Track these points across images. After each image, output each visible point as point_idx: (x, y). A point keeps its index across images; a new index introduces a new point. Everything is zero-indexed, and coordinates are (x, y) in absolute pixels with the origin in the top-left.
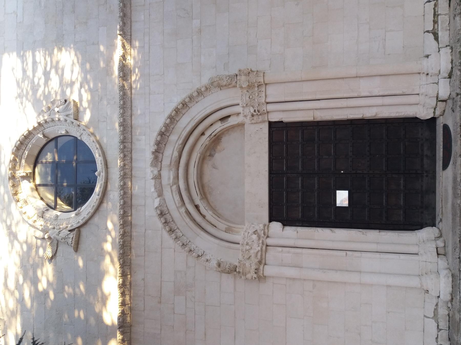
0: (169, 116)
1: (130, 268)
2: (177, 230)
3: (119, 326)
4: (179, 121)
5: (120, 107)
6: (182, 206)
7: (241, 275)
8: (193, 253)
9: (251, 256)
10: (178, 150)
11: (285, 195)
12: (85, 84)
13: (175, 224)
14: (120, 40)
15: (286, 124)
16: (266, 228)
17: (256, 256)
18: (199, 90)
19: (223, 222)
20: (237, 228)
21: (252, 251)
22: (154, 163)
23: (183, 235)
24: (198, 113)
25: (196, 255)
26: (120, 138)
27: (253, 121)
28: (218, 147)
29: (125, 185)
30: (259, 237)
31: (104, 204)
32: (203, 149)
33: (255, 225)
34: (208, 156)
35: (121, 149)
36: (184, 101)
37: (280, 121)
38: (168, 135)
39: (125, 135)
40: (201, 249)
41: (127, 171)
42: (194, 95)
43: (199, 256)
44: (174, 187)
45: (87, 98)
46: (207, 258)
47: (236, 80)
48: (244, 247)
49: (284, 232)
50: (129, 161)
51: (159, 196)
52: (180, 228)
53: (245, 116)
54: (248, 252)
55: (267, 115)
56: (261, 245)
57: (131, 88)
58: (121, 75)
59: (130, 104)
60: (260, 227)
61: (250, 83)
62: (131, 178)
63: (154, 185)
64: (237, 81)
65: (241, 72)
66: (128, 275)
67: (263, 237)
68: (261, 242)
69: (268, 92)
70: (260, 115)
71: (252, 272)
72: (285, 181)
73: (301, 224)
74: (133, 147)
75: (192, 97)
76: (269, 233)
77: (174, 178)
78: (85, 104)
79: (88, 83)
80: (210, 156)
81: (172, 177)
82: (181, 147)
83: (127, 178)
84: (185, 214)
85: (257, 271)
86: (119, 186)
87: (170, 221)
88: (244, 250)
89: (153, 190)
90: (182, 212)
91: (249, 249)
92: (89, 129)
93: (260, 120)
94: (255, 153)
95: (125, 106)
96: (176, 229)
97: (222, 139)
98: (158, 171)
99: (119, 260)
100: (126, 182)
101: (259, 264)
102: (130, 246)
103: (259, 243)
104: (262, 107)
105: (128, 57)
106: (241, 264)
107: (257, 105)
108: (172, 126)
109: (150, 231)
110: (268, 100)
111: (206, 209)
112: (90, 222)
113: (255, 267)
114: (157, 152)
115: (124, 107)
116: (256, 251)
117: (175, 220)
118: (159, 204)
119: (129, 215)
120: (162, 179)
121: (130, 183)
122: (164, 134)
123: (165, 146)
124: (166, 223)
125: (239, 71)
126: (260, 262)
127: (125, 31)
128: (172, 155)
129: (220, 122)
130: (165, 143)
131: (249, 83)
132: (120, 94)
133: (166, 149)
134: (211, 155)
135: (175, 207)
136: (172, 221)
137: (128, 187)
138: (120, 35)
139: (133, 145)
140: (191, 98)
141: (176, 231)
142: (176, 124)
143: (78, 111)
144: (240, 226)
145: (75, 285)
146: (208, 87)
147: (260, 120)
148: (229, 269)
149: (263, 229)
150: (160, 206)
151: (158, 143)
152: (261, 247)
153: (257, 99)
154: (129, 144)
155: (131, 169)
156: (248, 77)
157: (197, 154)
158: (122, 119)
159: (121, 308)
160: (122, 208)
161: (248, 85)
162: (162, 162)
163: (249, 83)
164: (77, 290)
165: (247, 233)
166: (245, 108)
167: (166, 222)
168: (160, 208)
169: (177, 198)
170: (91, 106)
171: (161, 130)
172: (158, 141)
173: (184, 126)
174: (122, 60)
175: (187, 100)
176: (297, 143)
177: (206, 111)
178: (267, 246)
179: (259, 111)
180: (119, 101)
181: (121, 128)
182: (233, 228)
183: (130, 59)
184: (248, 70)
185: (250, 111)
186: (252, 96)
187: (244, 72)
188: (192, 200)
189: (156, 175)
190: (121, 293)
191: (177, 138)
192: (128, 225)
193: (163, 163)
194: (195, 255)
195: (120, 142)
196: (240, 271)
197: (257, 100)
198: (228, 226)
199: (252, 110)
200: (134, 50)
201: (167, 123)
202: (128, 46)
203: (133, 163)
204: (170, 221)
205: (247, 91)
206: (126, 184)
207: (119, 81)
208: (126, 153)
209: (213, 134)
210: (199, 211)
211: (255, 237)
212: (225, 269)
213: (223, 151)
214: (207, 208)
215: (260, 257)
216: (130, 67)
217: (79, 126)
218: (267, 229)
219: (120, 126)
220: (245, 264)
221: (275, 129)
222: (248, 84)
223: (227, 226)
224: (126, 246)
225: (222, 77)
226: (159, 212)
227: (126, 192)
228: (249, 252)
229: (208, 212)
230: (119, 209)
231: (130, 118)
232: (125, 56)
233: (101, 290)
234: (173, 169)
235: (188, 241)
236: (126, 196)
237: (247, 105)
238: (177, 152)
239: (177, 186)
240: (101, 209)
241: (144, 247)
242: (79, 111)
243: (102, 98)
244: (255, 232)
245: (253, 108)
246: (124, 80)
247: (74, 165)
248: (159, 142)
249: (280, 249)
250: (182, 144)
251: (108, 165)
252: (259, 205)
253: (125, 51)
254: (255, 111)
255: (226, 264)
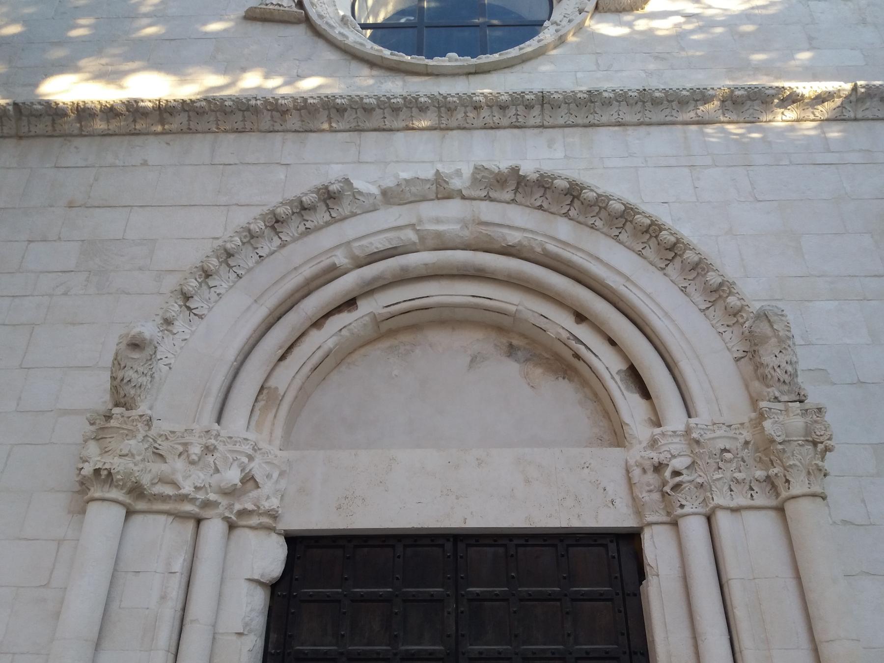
0: (632, 209)
1: (182, 132)
2: (277, 242)
3: (21, 104)
4: (617, 244)
5: (644, 90)
6: (354, 258)
7: (98, 422)
8: (198, 280)
9: (166, 463)
10: (525, 243)
11: (381, 590)
12: (697, 24)
13: (296, 235)
14: (839, 88)
15: (635, 595)
16: (266, 520)
17: (163, 480)
18: (729, 288)
19: (298, 382)
20: (273, 424)
21: (180, 464)
22: (483, 177)
23: (260, 257)
24: (649, 296)
25: (191, 289)
26: (555, 92)
27: (636, 472)
28: (539, 371)
29: (418, 110)
30: (230, 493)
31: (370, 70)
32: (533, 321)
33: (277, 482)
34: (510, 340)
35: (523, 97)
36: (687, 247)
37: (647, 569)
38: (573, 213)
39: (564, 109)
40: (210, 309)
41: (460, 115)
42: (709, 274)
43: (187, 297)
44: (411, 236)
45: (658, 29)
46: (176, 323)
47: (785, 398)
48: (199, 437)
49: (245, 586)
50: (488, 120)
51: (384, 193)
52: (285, 251)
53: (653, 443)
54: (178, 453)
55: (665, 519)
56: (198, 496)
57: (702, 122)
58: (737, 93)
59: (655, 119)
60: (268, 498)
61: (780, 447)
62: (441, 129)
63: (418, 178)
64: (780, 402)
65: (815, 417)
66: (163, 125)
67: (230, 507)
68: (212, 497)
69: (750, 517)
70: (664, 494)
71: (103, 460)
72: (429, 592)
73: (273, 651)
74: (529, 132)
75: (700, 271)
76: (247, 531)
77: (438, 235)
78: (642, 25)
79: (700, 29)
80: (511, 346)
81: (441, 228)
82: (534, 252)
83: (440, 117)
84: (326, 262)
85: (103, 477)
86: (417, 94)
87: (307, 221)
88: (188, 439)
89: (405, 175)
90: (335, 255)
91: (188, 456)
92: (574, 35)
93: (645, 497)
94: (527, 481)
95: (648, 105)
96: (280, 238)
97: (566, 380)
98: (460, 191)
99: (204, 99)
100: (429, 113)
101: (129, 484)
102: (246, 128)
103: (209, 490)
104: (694, 497)
105: (791, 114)
106: (135, 424)
107: (700, 480)
108: (599, 223)
109: (283, 177)
110: (723, 520)
111: (341, 330)
112: (321, 44)
113: (116, 470)
114: (518, 184)
115: (644, 102)
116: (179, 478)
117: (311, 238)
118: (360, 193)
119: (334, 125)
120: (436, 202)
121: (424, 124)
122: (576, 200)
123: (535, 208)
124: (303, 209)
125: (820, 409)
126: (137, 491)
127: (868, 104)
128: (509, 227)
129: (623, 366)
130: (545, 205)
131: (780, 443)
132: (681, 91)
133: (528, 210)
134: (511, 351)
135: (351, 238)
136: (308, 226)
137: (412, 121)
138: (855, 89)
139: (536, 131)
140: (699, 268)
141: (276, 238)
142: (606, 235)
143: (620, 12)
144: (279, 432)
145: (157, 17)
146: (742, 316)
147: (644, 494)
148: (122, 380)
149: (262, 507)
150: (354, 196)
151: (544, 183)
152: (193, 495)
153: (721, 476)
154: (538, 121)
155: (467, 126)
156: (803, 438)
157: (515, 305)
158: (612, 95)
159: (70, 107)
160: (354, 101)
161: (772, 441)
162: (487, 202)
163: (780, 443)
164: (145, 21)
165: (250, 452)
166: (682, 439)
167: (304, 208)
168: (349, 193)
169: (379, 243)
170: (637, 37)
171: (585, 188)
172: (552, 183)
173: (603, 256)
174: (780, 96)
175: (689, 255)
176: (569, 635)
177: (658, 317)
178: (199, 521)
179: (677, 487)
180: (663, 89)
181: (584, 93)
182: (274, 411)
183: (784, 118)
184: (828, 439)
185: (674, 457)
186: (730, 461)
187: (818, 426)
188: (371, 289)
189: (447, 183)
190: (112, 106)
191: (563, 237)
192: (303, 123)
193: (484, 205)
194: (191, 284)
195: (542, 92)
196: (112, 421)
197: (716, 476)
198: (283, 396)
199: (679, 463)
200: (815, 128)
201: (608, 203)
202: (824, 110)
203: (483, 131)
204: (307, 221)
205: (747, 443)
206: (423, 114)
207: (720, 88)
208: (512, 112)
209: (582, 348)
210: (339, 309)
211: (233, 476)
212: (122, 366)
213: (529, 384)
214: (345, 332)
215: (156, 492)
216: (761, 118)
217: (581, 11)
218: (260, 524)
219: (590, 91)
220: (135, 436)
221: (616, 555)
222: (779, 439)
223: (281, 391)
224: (244, 117)
225: (789, 349)
226: (334, 188)
227: (398, 115)
228: (180, 455)
229: (333, 335)
230: (350, 96)
231: (614, 121)
232: (794, 102)
233: (134, 71)
234: (466, 233)
235: (240, 272)
236: (386, 115)
237: (695, 446)
238: (519, 241)
239: (414, 243)
240: (354, 65)
241: (237, 162)
242: (621, 15)
243: (663, 59)
244: (249, 480)
245: (687, 468)
246: (723, 101)
247: (477, 21)
248: (547, 186)
249: (179, 564)
250: (546, 253)
251: (477, 75)
252: (346, 498)
253: (807, 104)
254: (676, 473)
255: (141, 369)
